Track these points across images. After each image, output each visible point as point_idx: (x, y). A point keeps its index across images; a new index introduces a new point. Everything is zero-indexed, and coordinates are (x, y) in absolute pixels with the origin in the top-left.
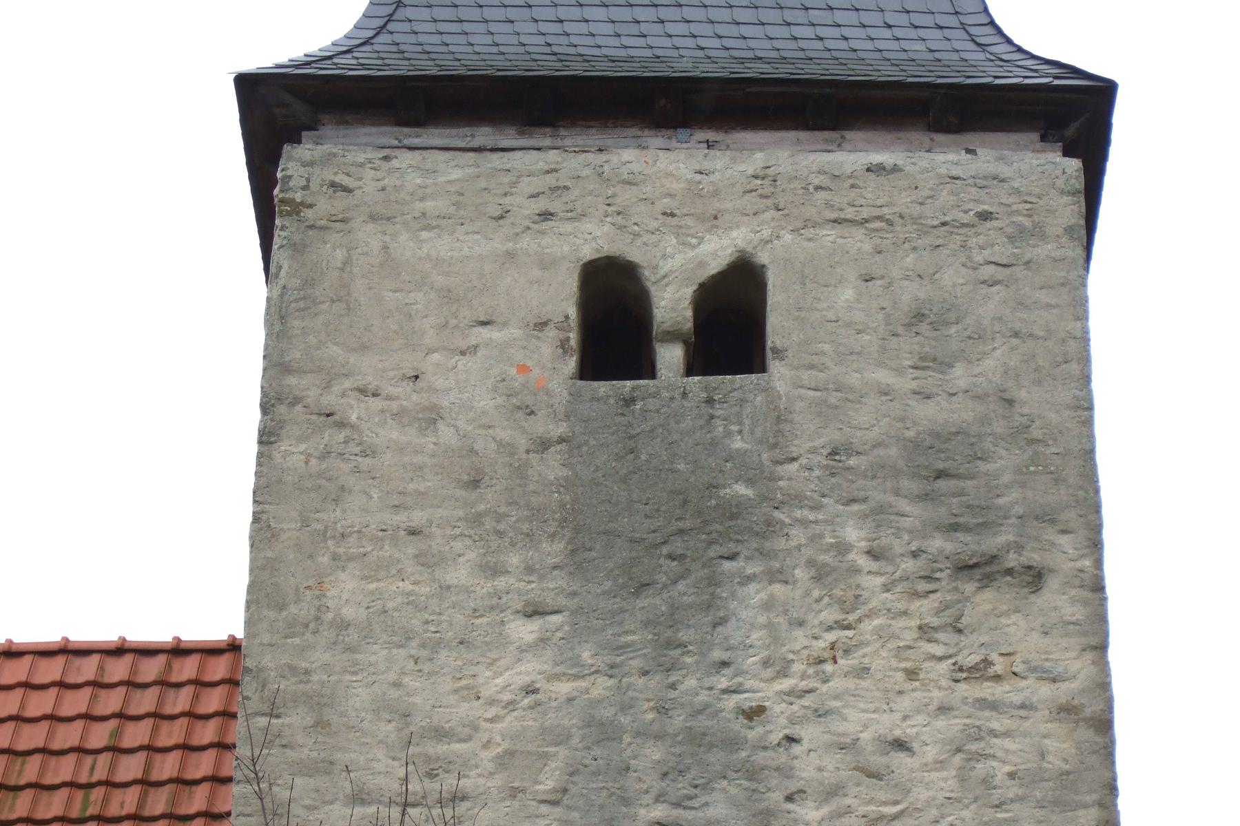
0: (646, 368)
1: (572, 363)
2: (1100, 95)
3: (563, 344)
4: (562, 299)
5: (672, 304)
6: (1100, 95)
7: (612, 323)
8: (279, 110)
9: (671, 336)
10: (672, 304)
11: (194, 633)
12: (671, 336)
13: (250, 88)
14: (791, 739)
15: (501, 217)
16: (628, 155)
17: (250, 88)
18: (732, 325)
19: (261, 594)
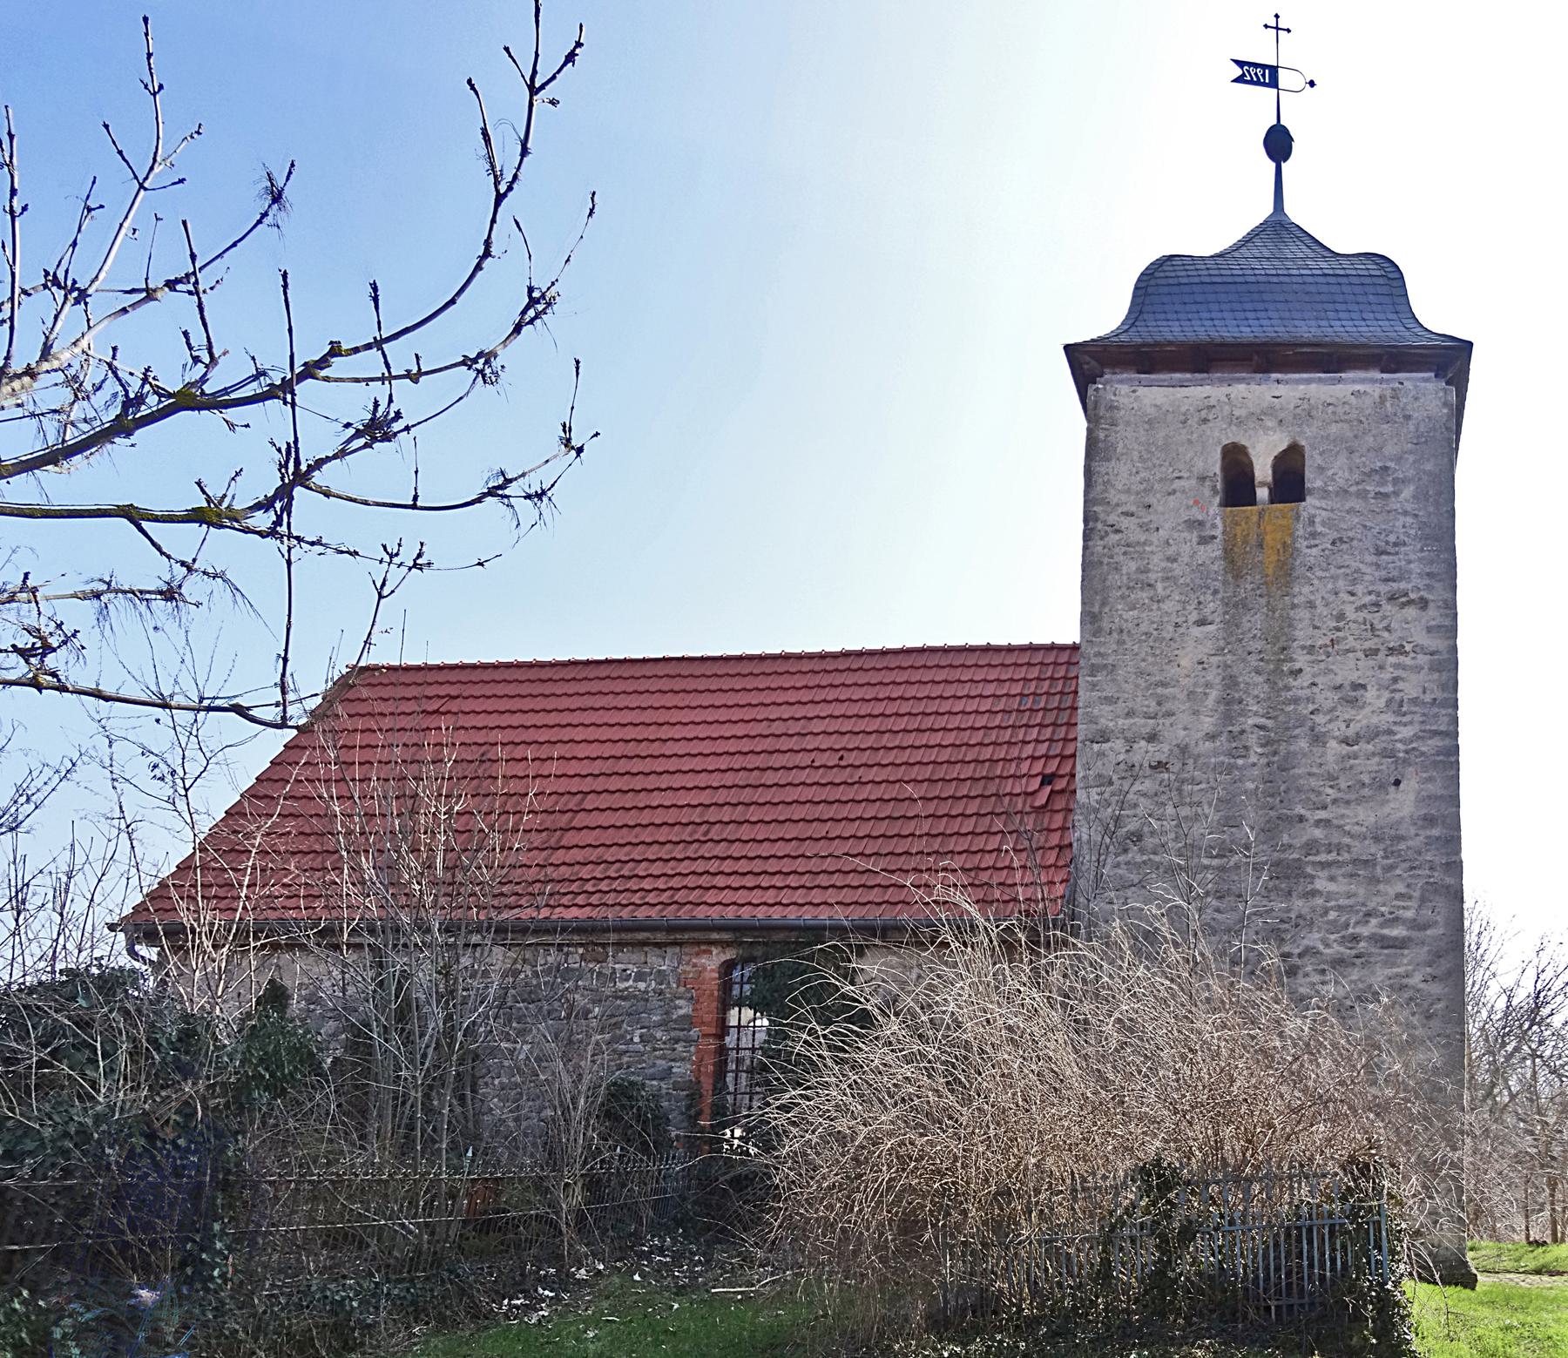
0: (1251, 500)
1: (1217, 500)
2: (1463, 349)
3: (1214, 488)
4: (1214, 464)
5: (1263, 470)
6: (1463, 349)
7: (1237, 483)
8: (1089, 363)
9: (1263, 484)
10: (1263, 470)
11: (1060, 641)
12: (1263, 484)
13: (1073, 352)
14: (1314, 684)
15: (567, 443)
16: (1242, 387)
17: (1073, 352)
18: (1290, 480)
19: (1090, 618)
